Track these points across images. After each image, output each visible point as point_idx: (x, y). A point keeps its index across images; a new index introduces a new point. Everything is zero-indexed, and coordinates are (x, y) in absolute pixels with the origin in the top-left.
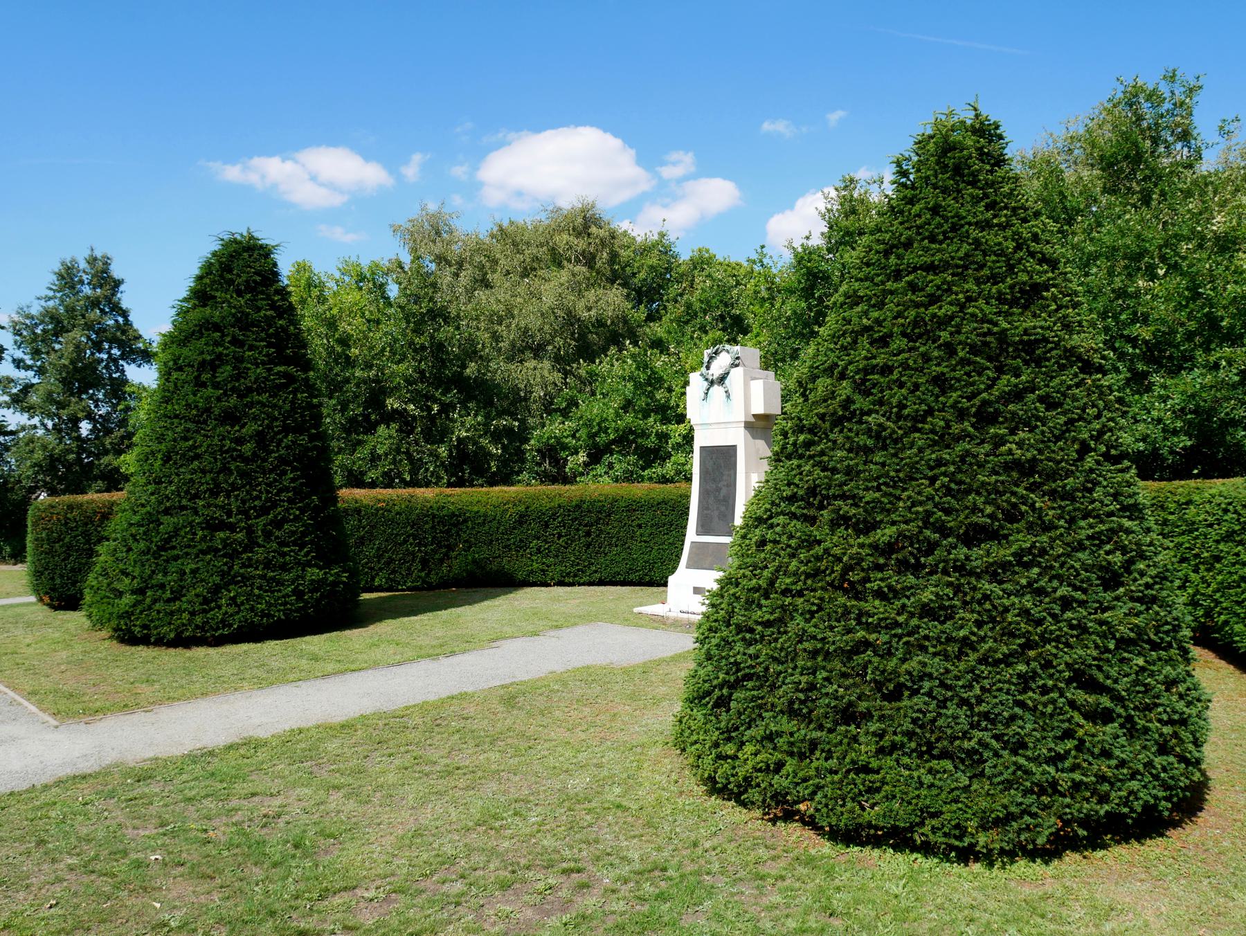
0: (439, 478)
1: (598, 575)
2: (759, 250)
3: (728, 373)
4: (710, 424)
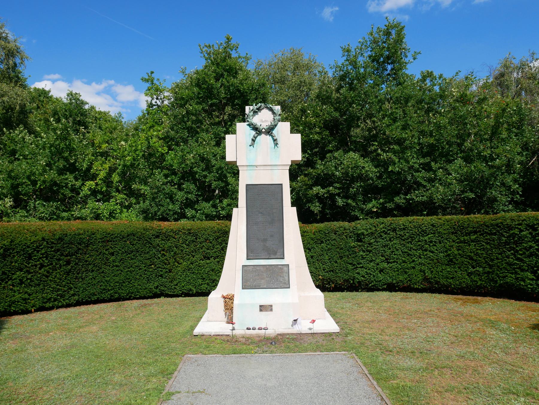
1: (76, 298)
2: (150, 74)
3: (276, 125)
4: (256, 166)
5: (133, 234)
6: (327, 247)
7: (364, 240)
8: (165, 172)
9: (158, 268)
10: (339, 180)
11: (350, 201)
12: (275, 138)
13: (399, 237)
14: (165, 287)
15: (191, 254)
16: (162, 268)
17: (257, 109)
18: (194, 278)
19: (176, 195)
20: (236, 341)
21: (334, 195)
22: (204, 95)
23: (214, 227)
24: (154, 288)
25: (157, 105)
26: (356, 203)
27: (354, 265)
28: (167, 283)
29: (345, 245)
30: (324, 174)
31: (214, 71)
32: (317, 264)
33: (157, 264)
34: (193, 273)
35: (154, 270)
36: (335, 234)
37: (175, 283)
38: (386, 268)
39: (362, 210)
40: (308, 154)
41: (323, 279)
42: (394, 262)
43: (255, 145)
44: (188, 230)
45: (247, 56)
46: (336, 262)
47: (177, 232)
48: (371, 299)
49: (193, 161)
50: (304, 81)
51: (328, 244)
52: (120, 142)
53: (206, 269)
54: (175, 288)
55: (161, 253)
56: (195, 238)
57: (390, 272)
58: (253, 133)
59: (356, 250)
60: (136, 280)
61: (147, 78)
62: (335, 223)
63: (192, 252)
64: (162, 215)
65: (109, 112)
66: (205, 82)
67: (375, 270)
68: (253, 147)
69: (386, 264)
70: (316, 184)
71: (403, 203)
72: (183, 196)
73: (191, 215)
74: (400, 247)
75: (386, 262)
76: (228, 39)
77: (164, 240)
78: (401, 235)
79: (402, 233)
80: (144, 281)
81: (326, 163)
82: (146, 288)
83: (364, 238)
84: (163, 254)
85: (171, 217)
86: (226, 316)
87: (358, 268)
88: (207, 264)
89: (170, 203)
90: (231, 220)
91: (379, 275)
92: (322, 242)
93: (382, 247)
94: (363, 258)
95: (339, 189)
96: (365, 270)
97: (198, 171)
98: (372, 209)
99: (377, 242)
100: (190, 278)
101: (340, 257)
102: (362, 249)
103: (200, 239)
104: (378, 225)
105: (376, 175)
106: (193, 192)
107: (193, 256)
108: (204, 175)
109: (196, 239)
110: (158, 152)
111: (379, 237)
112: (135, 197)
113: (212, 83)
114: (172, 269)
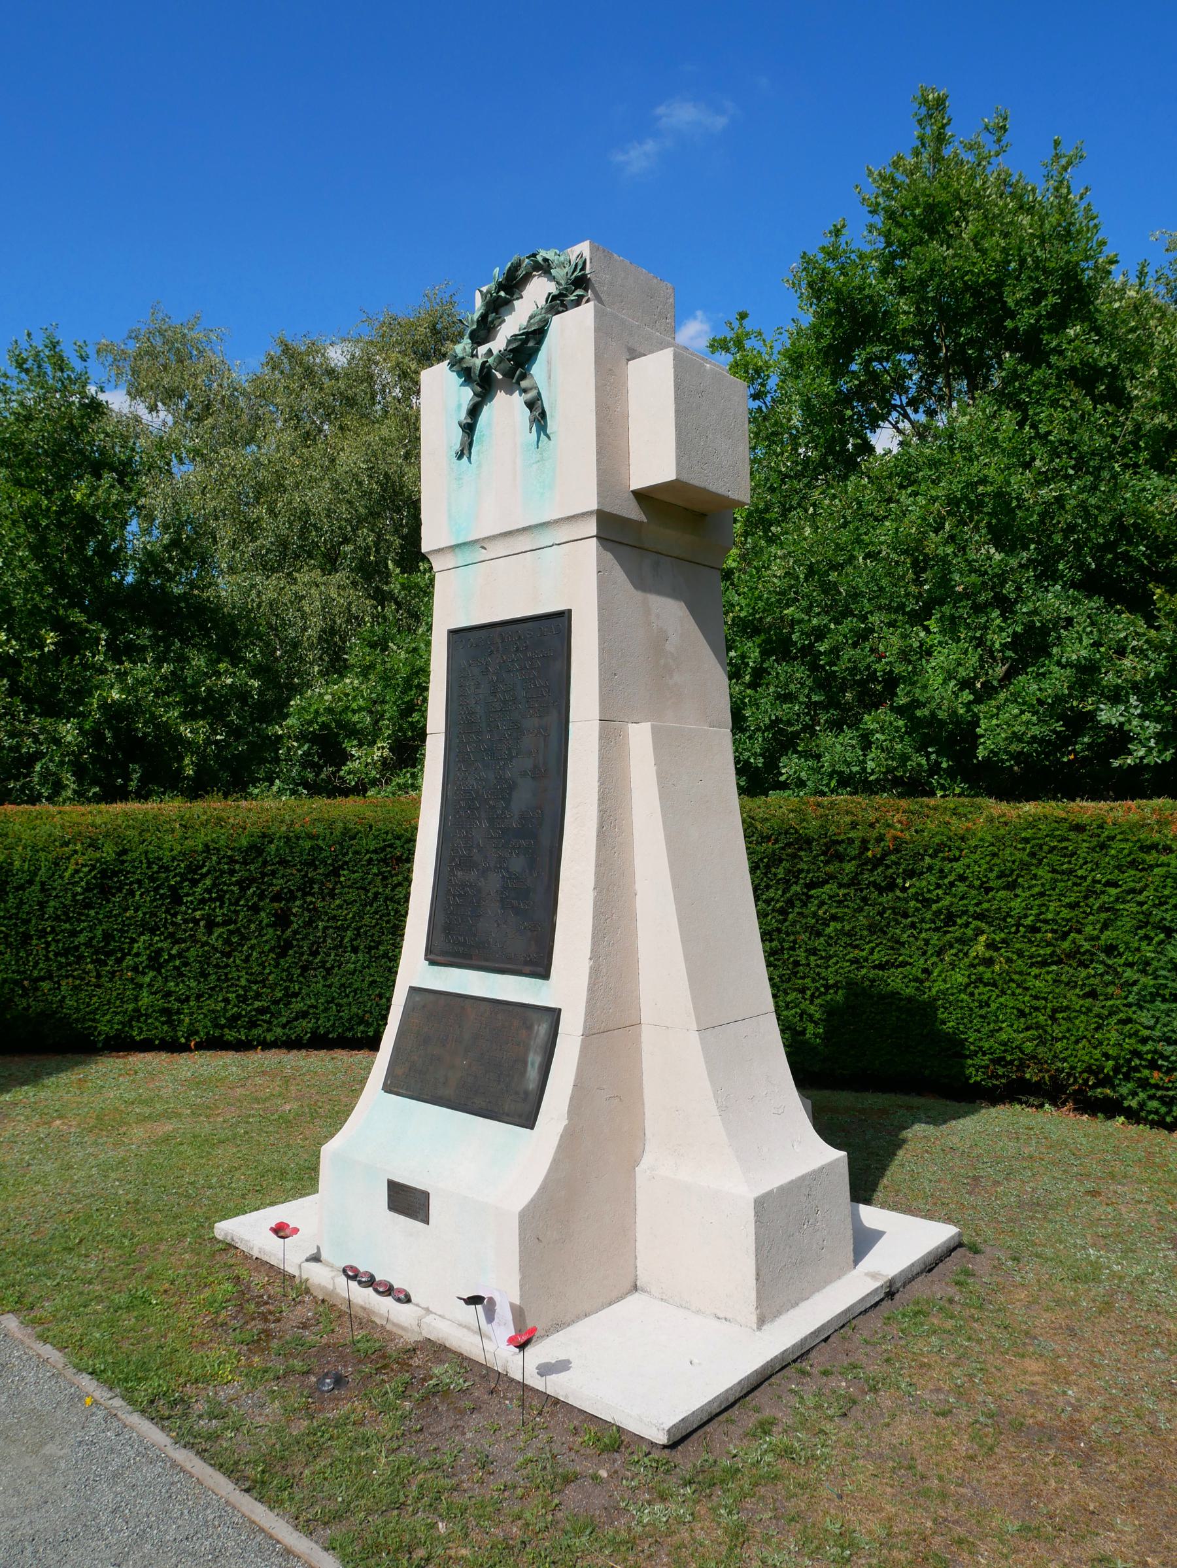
0: (58, 787)
1: (306, 1025)
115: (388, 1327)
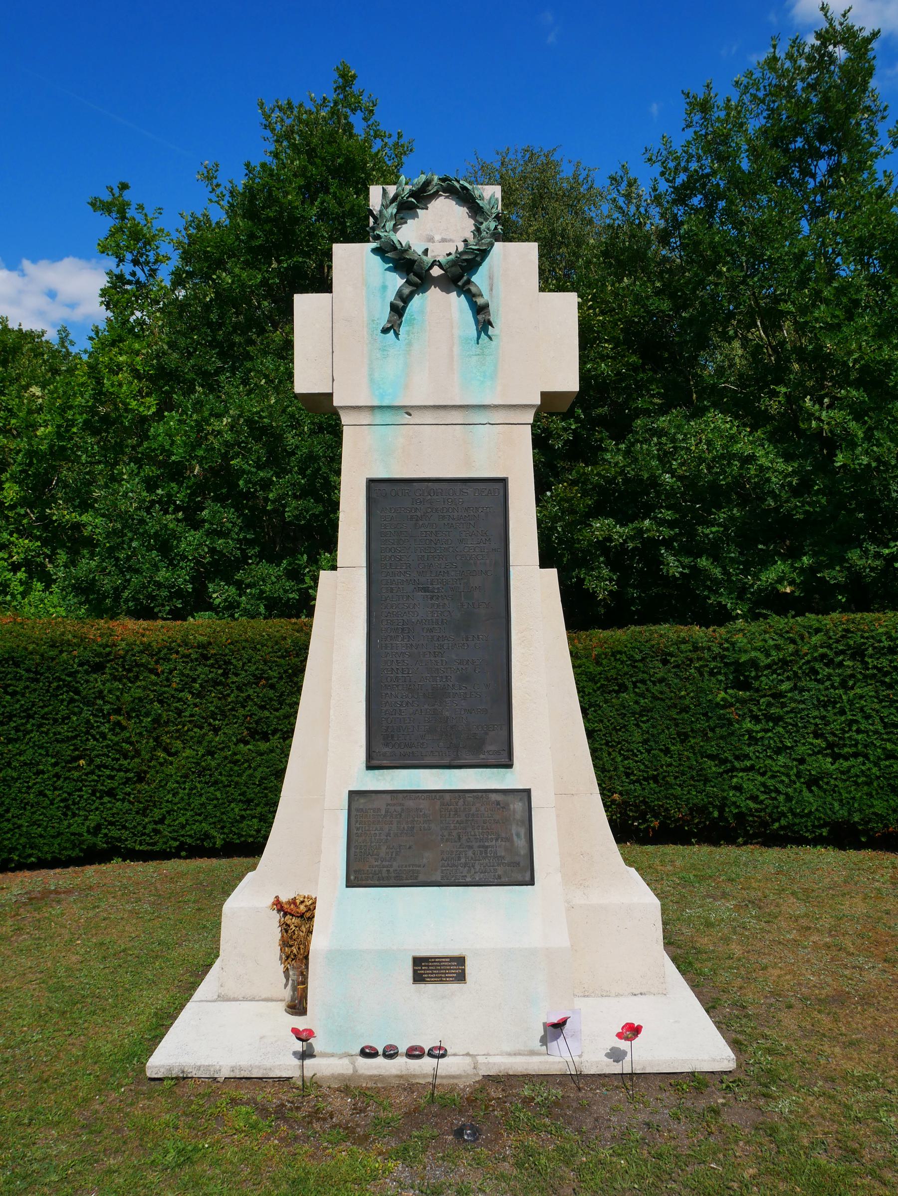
2: (116, 191)
3: (484, 253)
4: (408, 410)
5: (13, 658)
6: (637, 702)
7: (756, 684)
8: (149, 470)
9: (98, 767)
10: (671, 499)
11: (704, 562)
12: (480, 301)
13: (873, 676)
14: (124, 827)
15: (210, 724)
16: (113, 769)
17: (412, 194)
18: (217, 799)
19: (179, 539)
20: (316, 1115)
21: (653, 544)
22: (267, 241)
23: (285, 639)
24: (88, 832)
25: (138, 282)
26: (724, 568)
27: (725, 761)
28: (130, 817)
29: (697, 697)
30: (626, 481)
31: (302, 172)
32: (605, 754)
33: (97, 756)
34: (216, 782)
35: (86, 774)
36: (665, 662)
37: (157, 814)
38: (830, 775)
39: (741, 592)
40: (577, 420)
41: (625, 803)
42: (855, 755)
43: (403, 330)
44: (201, 646)
45: (402, 141)
46: (667, 751)
47: (162, 655)
48: (793, 881)
49: (228, 436)
50: (564, 230)
51: (642, 695)
52: (26, 387)
53: (255, 770)
54: (156, 831)
55: (109, 722)
56: (220, 671)
57: (840, 784)
58: (397, 281)
59: (731, 713)
60: (25, 809)
61: (107, 198)
62: (664, 628)
63: (213, 716)
64: (134, 599)
65: (43, 332)
66: (271, 200)
67: (793, 778)
68: (397, 335)
69: (830, 760)
70: (597, 511)
71: (872, 569)
72: (200, 545)
73: (225, 600)
74: (877, 707)
75: (827, 755)
76: (343, 76)
77: (120, 680)
78: (880, 670)
79: (884, 662)
80: (53, 811)
81: (633, 444)
82: (59, 834)
83: (757, 678)
84: (118, 723)
85: (163, 605)
86: (287, 980)
87: (736, 770)
88: (261, 754)
89: (161, 564)
90: (311, 613)
91: (806, 793)
92: (623, 688)
93: (816, 707)
94: (753, 740)
95: (671, 524)
96: (759, 778)
97: (245, 467)
98: (779, 587)
99: (802, 690)
100: (203, 799)
101: (679, 734)
102: (751, 711)
103: (237, 675)
104: (802, 638)
105: (790, 483)
106: (230, 531)
107: (216, 730)
108: (262, 479)
109: (225, 674)
110: (127, 410)
111: (807, 675)
112: (68, 547)
113: (290, 202)
114: (146, 772)
115: (438, 1081)
